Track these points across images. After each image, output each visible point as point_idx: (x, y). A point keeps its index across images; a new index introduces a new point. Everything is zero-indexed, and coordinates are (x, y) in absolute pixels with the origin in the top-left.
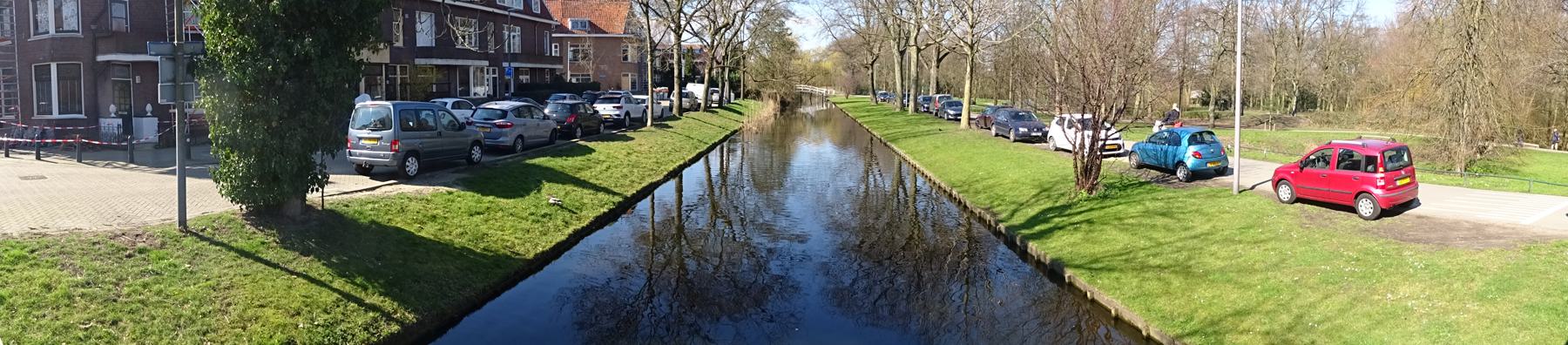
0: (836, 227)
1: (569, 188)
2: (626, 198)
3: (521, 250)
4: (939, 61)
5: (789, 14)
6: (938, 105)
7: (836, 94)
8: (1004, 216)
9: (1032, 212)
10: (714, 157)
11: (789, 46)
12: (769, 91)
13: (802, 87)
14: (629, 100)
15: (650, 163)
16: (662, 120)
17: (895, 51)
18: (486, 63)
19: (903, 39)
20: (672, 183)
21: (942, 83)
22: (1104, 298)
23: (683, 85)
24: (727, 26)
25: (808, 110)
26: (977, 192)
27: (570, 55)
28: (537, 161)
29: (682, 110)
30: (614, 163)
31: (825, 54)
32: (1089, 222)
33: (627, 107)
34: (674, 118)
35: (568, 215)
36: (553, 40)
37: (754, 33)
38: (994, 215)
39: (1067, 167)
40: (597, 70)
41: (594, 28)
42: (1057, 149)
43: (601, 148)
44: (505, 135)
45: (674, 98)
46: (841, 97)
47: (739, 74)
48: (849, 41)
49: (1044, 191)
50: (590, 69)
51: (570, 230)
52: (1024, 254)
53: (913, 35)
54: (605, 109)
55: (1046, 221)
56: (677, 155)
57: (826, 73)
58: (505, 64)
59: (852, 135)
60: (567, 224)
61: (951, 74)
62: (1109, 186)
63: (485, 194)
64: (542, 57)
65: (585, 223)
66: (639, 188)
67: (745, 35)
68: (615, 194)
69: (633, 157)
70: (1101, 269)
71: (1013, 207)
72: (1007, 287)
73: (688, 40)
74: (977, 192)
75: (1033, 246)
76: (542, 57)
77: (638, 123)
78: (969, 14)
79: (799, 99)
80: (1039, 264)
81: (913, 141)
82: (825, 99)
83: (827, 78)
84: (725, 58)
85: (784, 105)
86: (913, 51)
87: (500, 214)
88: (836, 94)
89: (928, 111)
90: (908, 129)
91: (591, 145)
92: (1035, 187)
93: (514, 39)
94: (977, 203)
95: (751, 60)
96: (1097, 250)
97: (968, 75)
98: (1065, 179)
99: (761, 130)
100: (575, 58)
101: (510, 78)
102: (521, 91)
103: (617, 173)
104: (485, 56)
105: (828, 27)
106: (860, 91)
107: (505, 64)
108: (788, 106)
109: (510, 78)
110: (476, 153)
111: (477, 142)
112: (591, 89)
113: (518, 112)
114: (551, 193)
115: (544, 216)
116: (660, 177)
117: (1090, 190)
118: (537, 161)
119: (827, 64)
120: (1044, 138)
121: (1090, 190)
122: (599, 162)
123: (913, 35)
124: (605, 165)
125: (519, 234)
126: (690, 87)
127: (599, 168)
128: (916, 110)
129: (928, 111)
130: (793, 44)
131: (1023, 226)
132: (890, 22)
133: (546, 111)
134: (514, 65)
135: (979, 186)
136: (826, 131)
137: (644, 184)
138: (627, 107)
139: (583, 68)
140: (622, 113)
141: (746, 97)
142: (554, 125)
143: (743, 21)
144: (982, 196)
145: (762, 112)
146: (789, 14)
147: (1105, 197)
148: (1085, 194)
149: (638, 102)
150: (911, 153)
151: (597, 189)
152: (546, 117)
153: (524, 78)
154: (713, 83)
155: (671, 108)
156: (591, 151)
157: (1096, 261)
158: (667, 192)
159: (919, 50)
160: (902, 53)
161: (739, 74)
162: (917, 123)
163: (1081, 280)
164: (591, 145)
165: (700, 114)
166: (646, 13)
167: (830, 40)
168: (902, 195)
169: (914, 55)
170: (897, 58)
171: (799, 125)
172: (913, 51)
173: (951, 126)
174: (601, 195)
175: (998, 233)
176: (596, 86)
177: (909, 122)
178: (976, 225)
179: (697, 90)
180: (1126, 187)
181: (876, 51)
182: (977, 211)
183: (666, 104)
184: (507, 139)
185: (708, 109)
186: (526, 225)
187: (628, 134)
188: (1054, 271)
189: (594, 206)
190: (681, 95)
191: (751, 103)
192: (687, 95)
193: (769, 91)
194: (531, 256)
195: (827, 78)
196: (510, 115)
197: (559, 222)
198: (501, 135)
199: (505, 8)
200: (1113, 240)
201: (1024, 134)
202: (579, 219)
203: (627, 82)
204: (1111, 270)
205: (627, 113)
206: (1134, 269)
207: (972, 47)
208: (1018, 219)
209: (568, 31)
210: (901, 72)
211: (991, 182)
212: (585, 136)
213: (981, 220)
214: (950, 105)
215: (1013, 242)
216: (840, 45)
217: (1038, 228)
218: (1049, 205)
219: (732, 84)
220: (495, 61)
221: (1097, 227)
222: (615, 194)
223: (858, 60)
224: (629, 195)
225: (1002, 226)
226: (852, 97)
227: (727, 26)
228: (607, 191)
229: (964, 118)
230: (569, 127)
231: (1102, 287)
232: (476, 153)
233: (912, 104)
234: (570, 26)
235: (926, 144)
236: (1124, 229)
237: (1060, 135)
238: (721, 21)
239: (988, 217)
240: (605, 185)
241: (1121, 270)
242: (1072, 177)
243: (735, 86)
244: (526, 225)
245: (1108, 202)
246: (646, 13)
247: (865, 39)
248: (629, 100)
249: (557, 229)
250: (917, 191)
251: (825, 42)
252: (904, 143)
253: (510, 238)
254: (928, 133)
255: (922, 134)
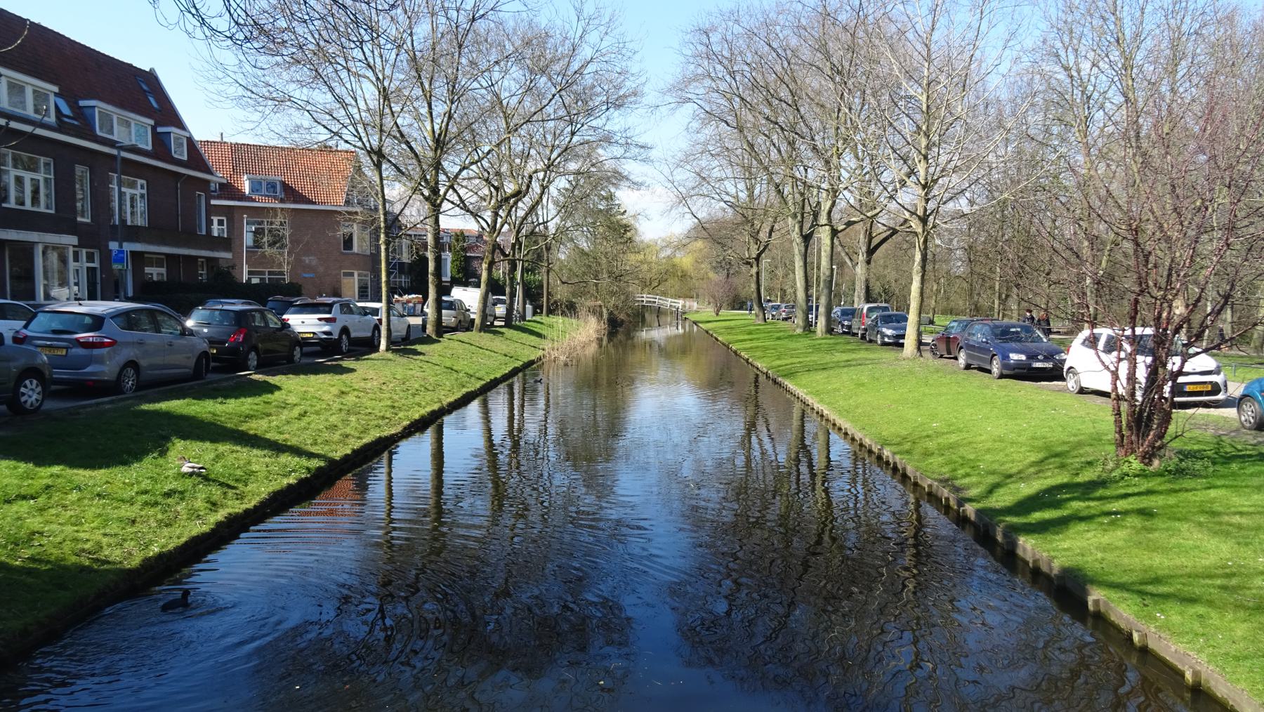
0: (694, 515)
1: (223, 448)
2: (332, 462)
3: (115, 554)
4: (871, 252)
5: (618, 177)
6: (868, 323)
7: (703, 311)
8: (973, 492)
9: (1026, 489)
10: (499, 403)
11: (620, 231)
12: (590, 303)
13: (646, 298)
14: (347, 308)
15: (380, 408)
16: (405, 344)
17: (795, 235)
18: (73, 240)
19: (808, 218)
20: (428, 437)
21: (877, 288)
22: (1171, 648)
23: (443, 290)
24: (518, 195)
25: (657, 334)
26: (927, 454)
27: (248, 239)
28: (164, 406)
29: (441, 329)
30: (314, 411)
31: (681, 246)
32: (1145, 513)
33: (344, 320)
34: (428, 341)
35: (216, 492)
36: (212, 211)
37: (566, 209)
38: (957, 490)
39: (1103, 418)
40: (297, 265)
41: (290, 193)
42: (1082, 391)
43: (291, 386)
44: (100, 360)
45: (429, 309)
46: (708, 312)
47: (541, 276)
48: (721, 224)
49: (1054, 456)
50: (284, 265)
51: (220, 515)
52: (1009, 558)
53: (826, 206)
54: (304, 323)
55: (1057, 505)
56: (429, 396)
57: (684, 276)
58: (113, 246)
59: (730, 376)
60: (214, 506)
61: (891, 275)
62: (1185, 455)
63: (41, 461)
64: (190, 236)
65: (250, 504)
66: (357, 444)
67: (549, 214)
68: (311, 455)
69: (351, 399)
70: (1166, 597)
71: (991, 480)
72: (986, 615)
73: (453, 221)
74: (927, 454)
75: (1028, 546)
76: (190, 236)
77: (367, 346)
78: (921, 169)
79: (640, 316)
80: (1037, 575)
81: (820, 376)
82: (680, 316)
83: (685, 284)
84: (517, 244)
85: (614, 325)
86: (824, 235)
87: (74, 496)
88: (703, 311)
89: (849, 332)
90: (815, 358)
91: (272, 380)
92: (1034, 449)
93: (131, 200)
94: (928, 470)
95: (562, 254)
96: (1159, 562)
97: (917, 267)
98: (1097, 439)
99: (572, 362)
100: (257, 244)
101: (124, 268)
102: (145, 290)
103: (318, 423)
104: (73, 228)
105: (683, 199)
106: (738, 303)
107: (113, 246)
108: (622, 326)
109: (124, 268)
110: (31, 393)
111: (33, 372)
112: (287, 294)
113: (127, 320)
114: (185, 456)
115: (168, 495)
116: (399, 429)
117: (1147, 458)
118: (164, 406)
119: (685, 261)
120: (1056, 374)
121: (1147, 458)
122: (285, 406)
123: (826, 206)
124: (296, 412)
125: (114, 528)
126: (457, 293)
127: (285, 415)
128: (830, 330)
129: (849, 332)
130: (627, 228)
131: (1009, 511)
132: (787, 190)
133: (190, 323)
134: (129, 247)
135: (931, 445)
136: (684, 368)
137: (367, 439)
138: (344, 320)
139: (271, 261)
140: (335, 329)
141: (550, 312)
142: (204, 346)
143: (544, 188)
144: (936, 461)
145: (578, 334)
146: (618, 177)
147: (1180, 472)
148: (1136, 465)
149: (365, 312)
150: (817, 394)
151: (278, 448)
152: (185, 332)
153: (155, 272)
154: (495, 287)
155: (424, 327)
156: (279, 388)
157: (1157, 581)
158: (413, 458)
159: (834, 233)
160: (807, 238)
161: (541, 276)
162: (830, 350)
163: (1124, 611)
164: (272, 380)
165: (473, 336)
166: (378, 166)
167: (689, 222)
168: (804, 469)
169: (826, 240)
170: (797, 248)
171: (635, 357)
172: (824, 235)
173: (889, 355)
174: (285, 458)
175: (961, 521)
176: (294, 290)
177: (817, 349)
178: (930, 511)
179: (469, 297)
180: (1228, 459)
181: (763, 236)
182: (925, 484)
183: (417, 321)
184: (106, 368)
185: (487, 327)
186: (127, 511)
187: (346, 363)
188: (1067, 590)
189: (268, 475)
190: (440, 305)
191: (558, 321)
192: (451, 306)
193: (590, 303)
194: (135, 562)
195: (685, 284)
196: (110, 326)
197: (199, 504)
198: (90, 360)
199: (112, 144)
200: (1194, 548)
201: (1019, 365)
202: (240, 497)
203: (351, 285)
204: (1192, 600)
205: (345, 330)
206: (1238, 606)
207: (924, 220)
208: (1003, 499)
209: (242, 197)
210: (798, 267)
211: (953, 438)
212: (260, 368)
213: (933, 497)
214: (887, 320)
215: (990, 536)
216: (708, 231)
217: (1037, 516)
218: (1062, 478)
219: (526, 286)
220: (91, 238)
221: (1158, 523)
222: (311, 455)
223: (736, 257)
224: (337, 455)
225: (970, 509)
226: (726, 313)
227: (518, 195)
228: (297, 451)
229: (910, 341)
230: (234, 351)
231: (1166, 627)
232: (31, 393)
233: (822, 322)
234: (247, 189)
235: (842, 380)
236: (1223, 532)
237: (1087, 364)
238: (510, 188)
239: (945, 493)
240: (294, 441)
241: (1210, 603)
242: (1112, 435)
243: (533, 294)
244: (127, 511)
245: (1187, 483)
246: (378, 166)
247: (746, 216)
248: (347, 308)
249: (194, 515)
250: (828, 466)
251: (680, 226)
252: (805, 379)
253: (90, 535)
254: (848, 364)
255: (837, 365)
